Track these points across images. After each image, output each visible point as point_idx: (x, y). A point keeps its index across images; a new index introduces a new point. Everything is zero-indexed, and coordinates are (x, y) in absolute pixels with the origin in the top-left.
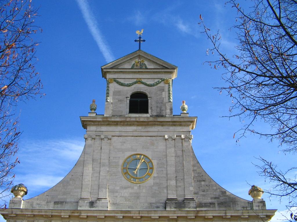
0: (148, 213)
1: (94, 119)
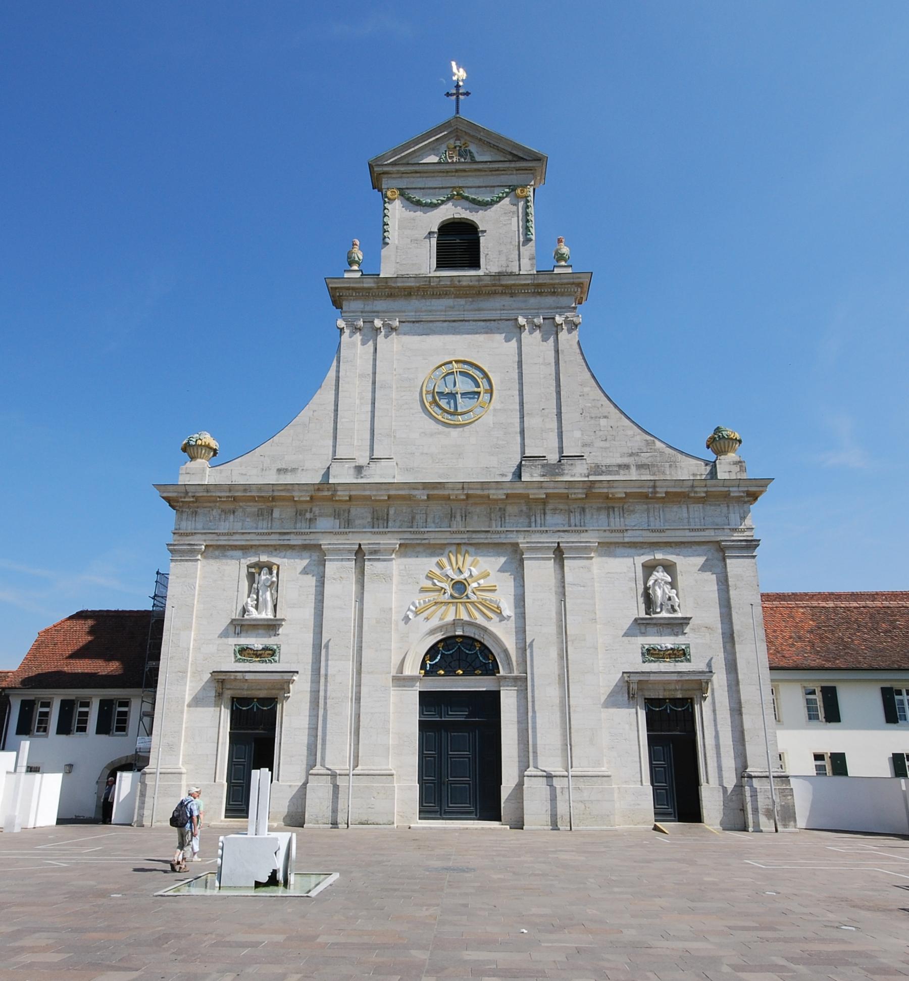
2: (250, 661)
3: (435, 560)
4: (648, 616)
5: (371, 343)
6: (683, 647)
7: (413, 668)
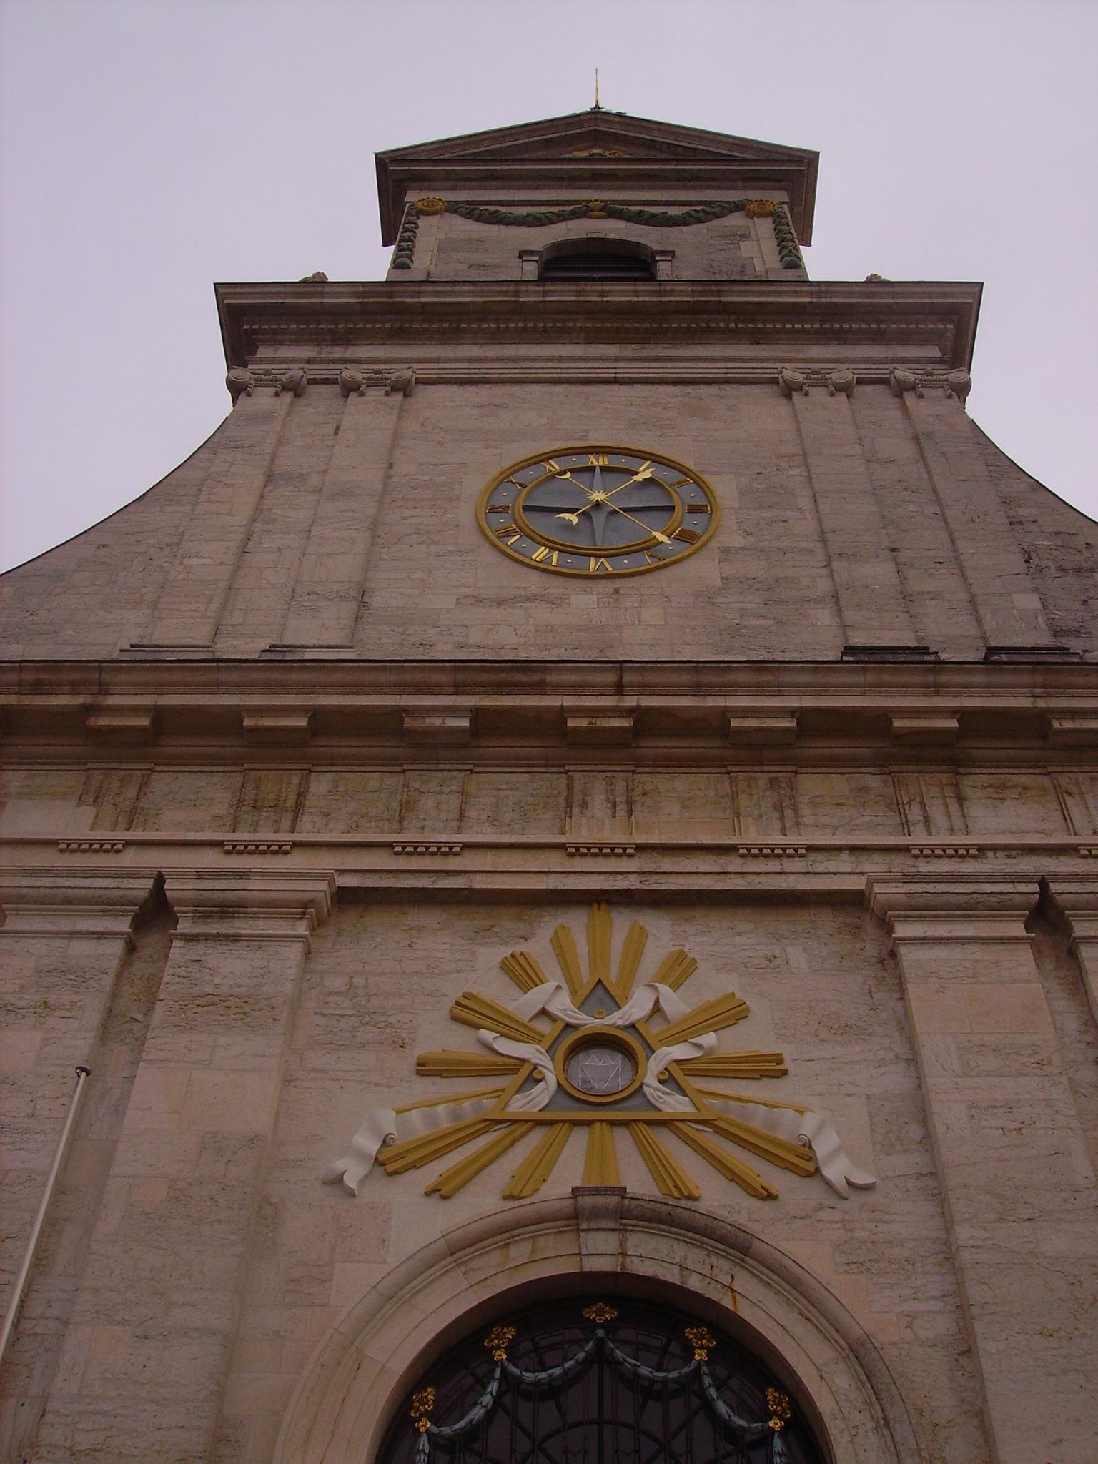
0: (698, 689)
1: (359, 688)
3: (492, 955)
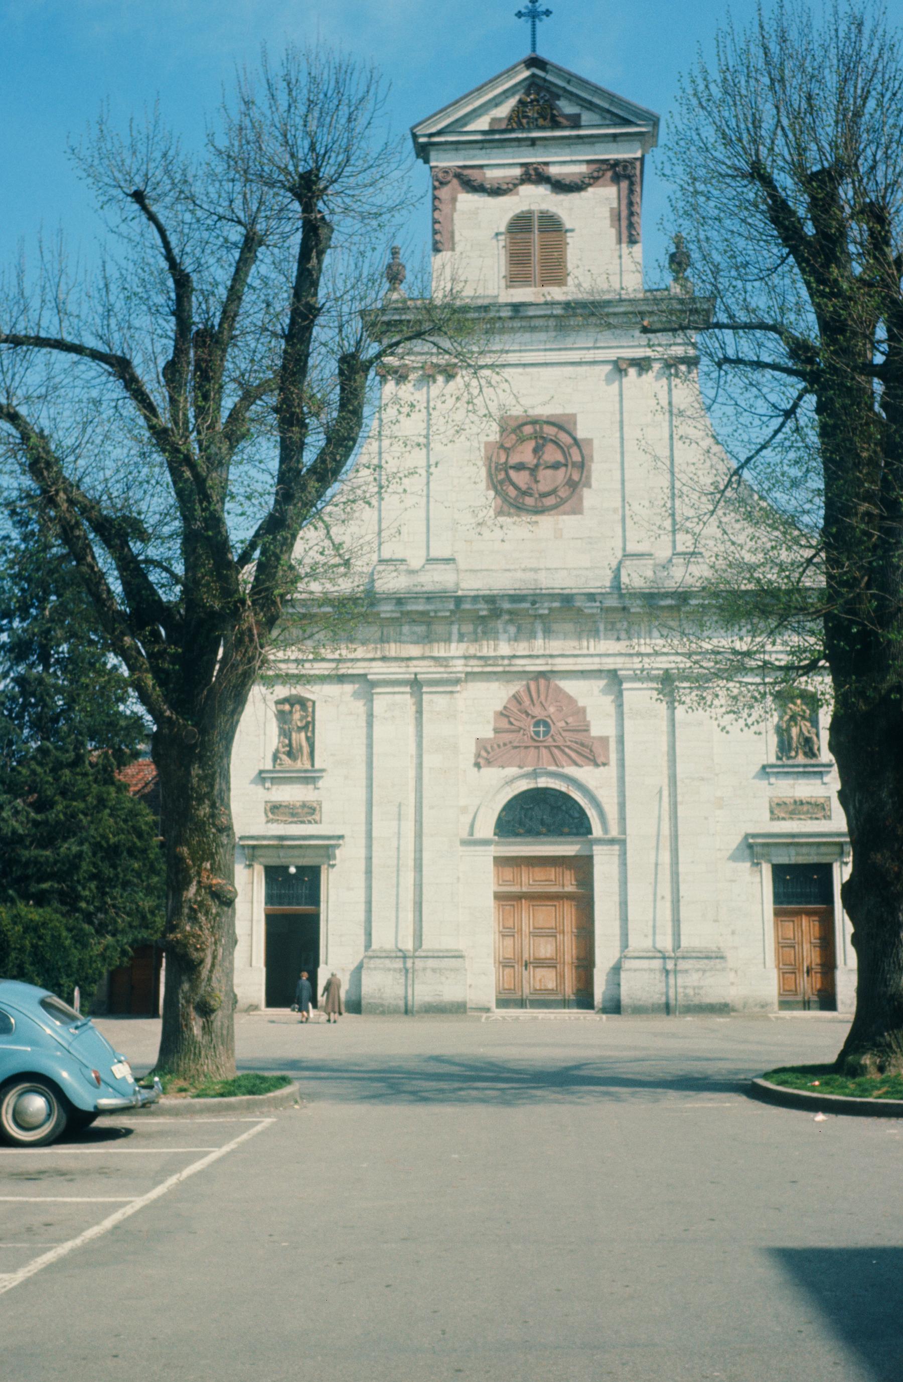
2: (285, 822)
4: (779, 763)
5: (616, 384)
6: (822, 800)
7: (486, 828)
